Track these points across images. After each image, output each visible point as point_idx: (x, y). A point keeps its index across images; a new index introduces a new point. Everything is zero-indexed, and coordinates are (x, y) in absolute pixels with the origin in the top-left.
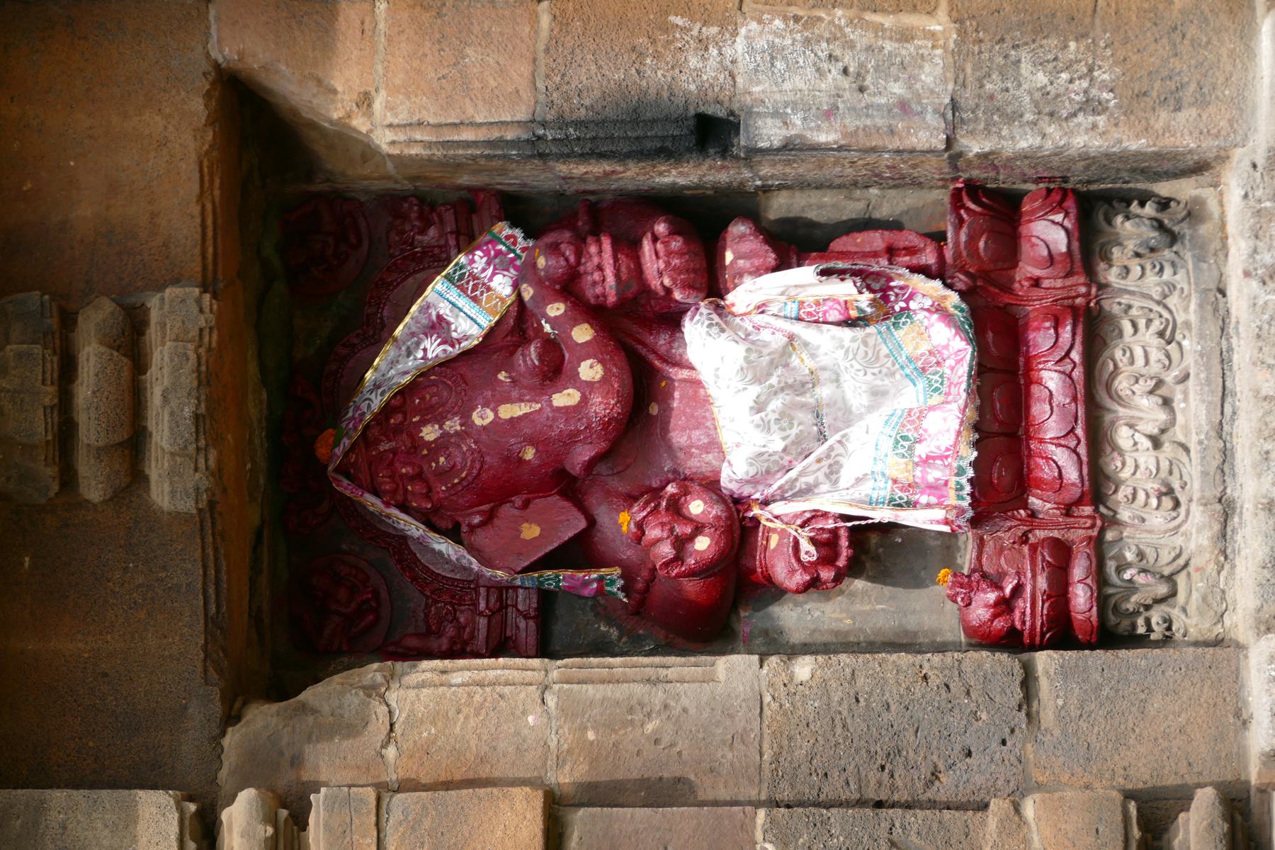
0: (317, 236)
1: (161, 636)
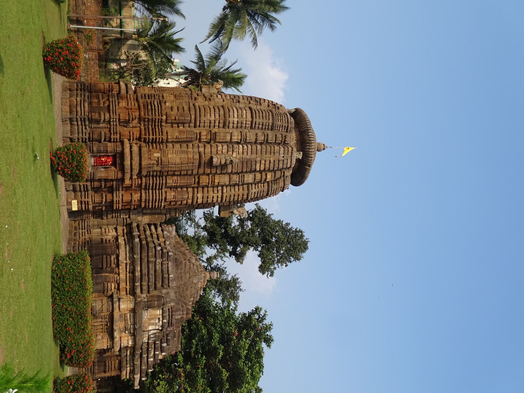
0: (114, 164)
1: (118, 155)
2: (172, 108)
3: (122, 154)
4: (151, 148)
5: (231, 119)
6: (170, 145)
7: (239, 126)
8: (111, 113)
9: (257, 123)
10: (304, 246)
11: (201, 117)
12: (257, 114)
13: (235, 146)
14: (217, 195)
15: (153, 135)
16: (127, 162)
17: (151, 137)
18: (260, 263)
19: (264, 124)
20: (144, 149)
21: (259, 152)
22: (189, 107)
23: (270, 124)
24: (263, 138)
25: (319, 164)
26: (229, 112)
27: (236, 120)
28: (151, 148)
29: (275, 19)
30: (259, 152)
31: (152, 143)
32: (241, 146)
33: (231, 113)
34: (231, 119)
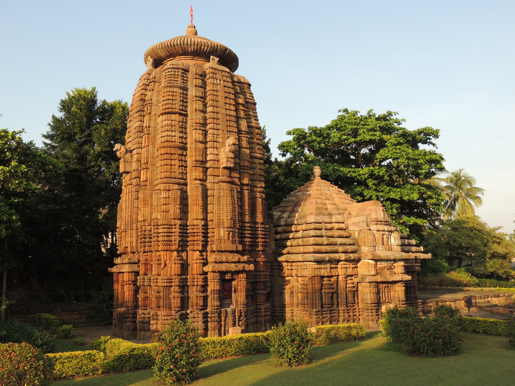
14: (257, 164)
19: (163, 162)
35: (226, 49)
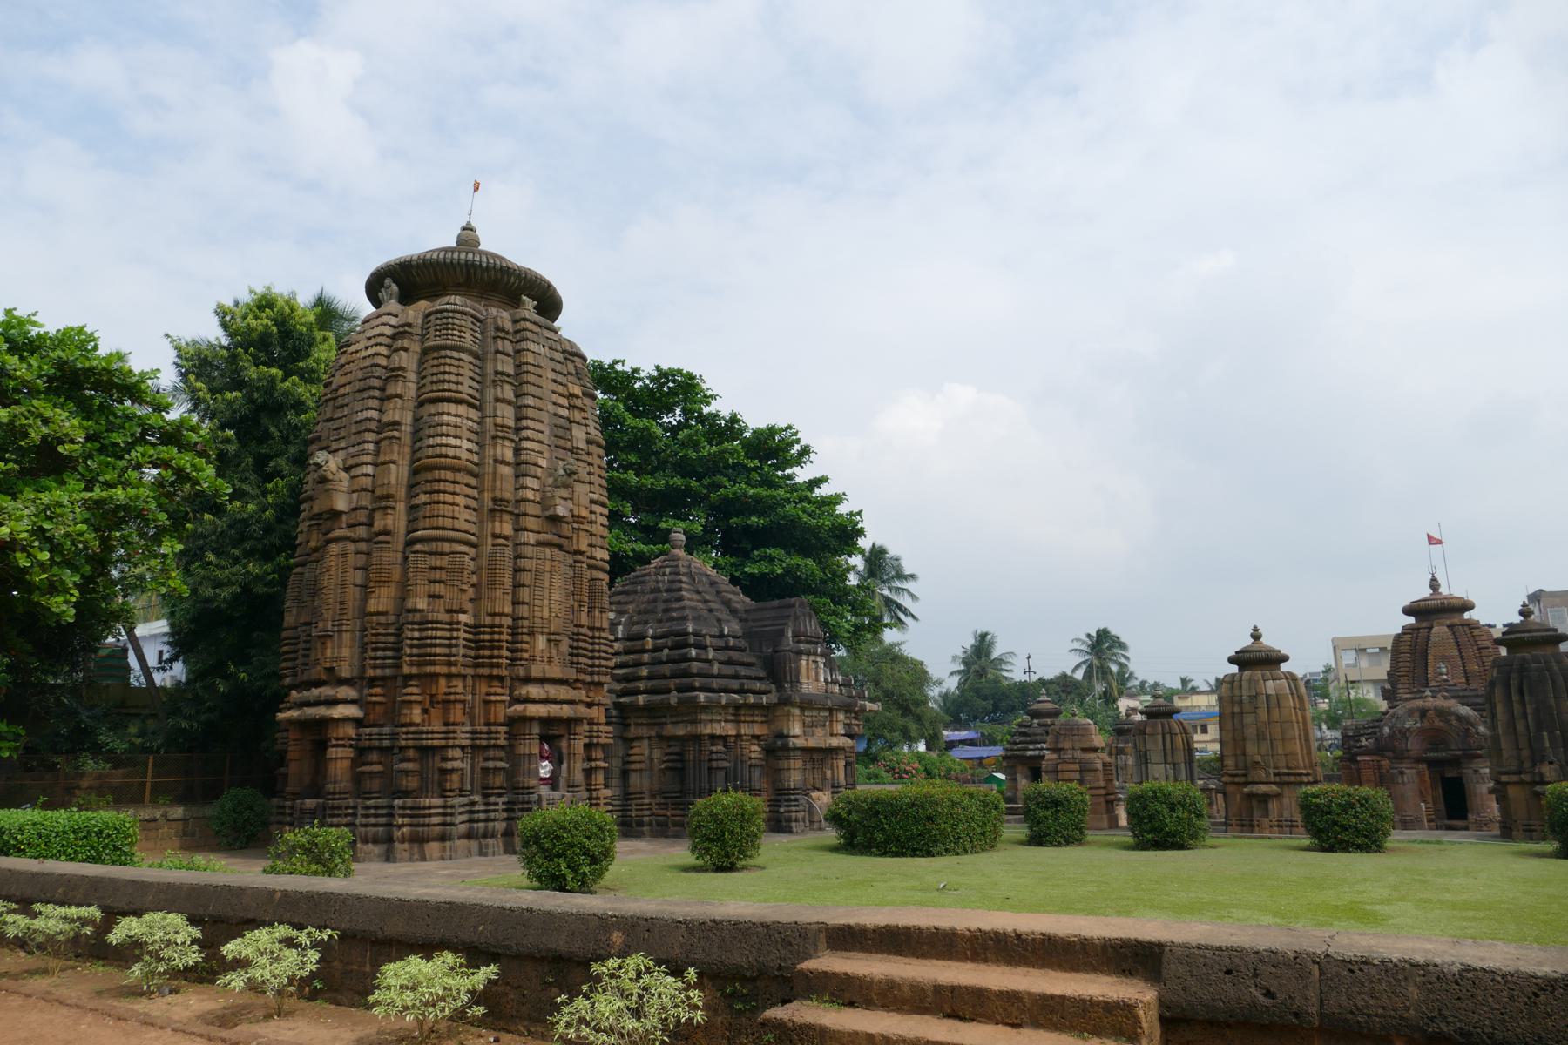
2: (430, 596)
3: (546, 722)
4: (526, 655)
5: (464, 455)
6: (523, 610)
7: (481, 439)
8: (451, 742)
9: (471, 391)
10: (1103, 635)
11: (457, 526)
12: (453, 387)
13: (523, 457)
15: (500, 648)
16: (566, 711)
17: (505, 653)
18: (591, 356)
20: (536, 671)
21: (538, 403)
22: (431, 553)
23: (472, 359)
24: (507, 387)
25: (505, 242)
26: (446, 456)
27: (466, 444)
28: (526, 655)
29: (906, 611)
30: (538, 403)
31: (517, 650)
32: (525, 444)
33: (451, 452)
34: (464, 455)
35: (550, 285)
